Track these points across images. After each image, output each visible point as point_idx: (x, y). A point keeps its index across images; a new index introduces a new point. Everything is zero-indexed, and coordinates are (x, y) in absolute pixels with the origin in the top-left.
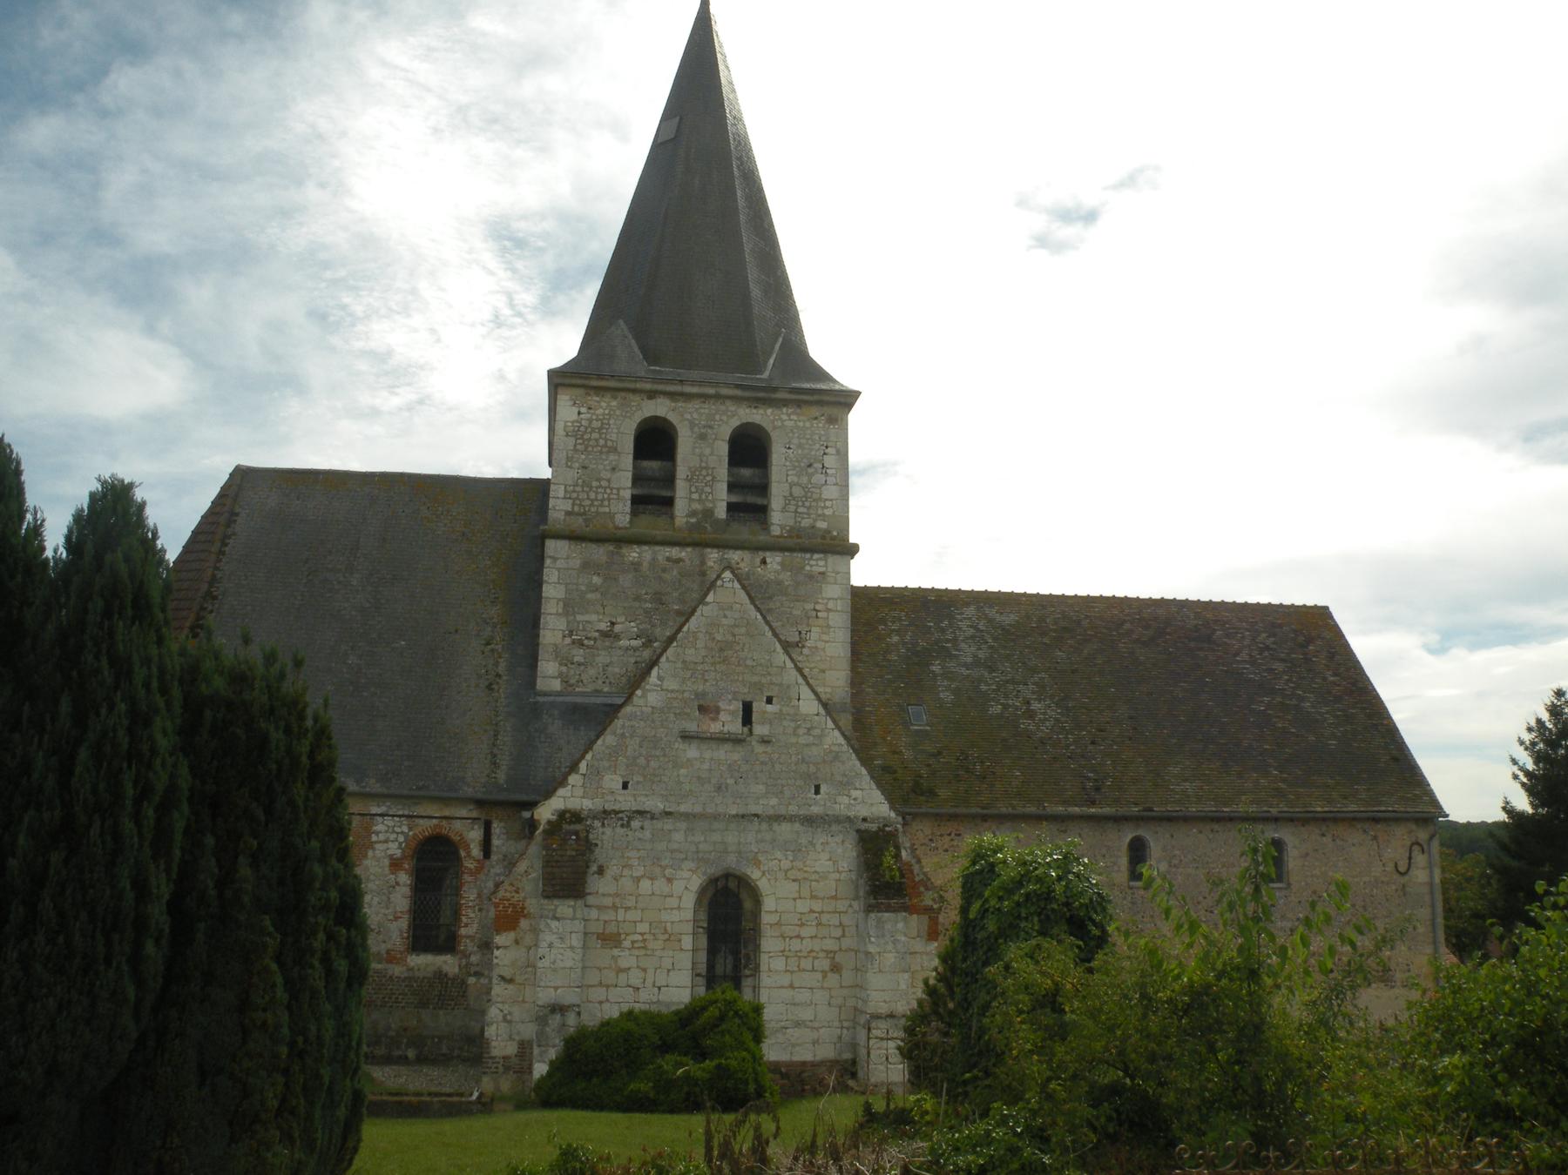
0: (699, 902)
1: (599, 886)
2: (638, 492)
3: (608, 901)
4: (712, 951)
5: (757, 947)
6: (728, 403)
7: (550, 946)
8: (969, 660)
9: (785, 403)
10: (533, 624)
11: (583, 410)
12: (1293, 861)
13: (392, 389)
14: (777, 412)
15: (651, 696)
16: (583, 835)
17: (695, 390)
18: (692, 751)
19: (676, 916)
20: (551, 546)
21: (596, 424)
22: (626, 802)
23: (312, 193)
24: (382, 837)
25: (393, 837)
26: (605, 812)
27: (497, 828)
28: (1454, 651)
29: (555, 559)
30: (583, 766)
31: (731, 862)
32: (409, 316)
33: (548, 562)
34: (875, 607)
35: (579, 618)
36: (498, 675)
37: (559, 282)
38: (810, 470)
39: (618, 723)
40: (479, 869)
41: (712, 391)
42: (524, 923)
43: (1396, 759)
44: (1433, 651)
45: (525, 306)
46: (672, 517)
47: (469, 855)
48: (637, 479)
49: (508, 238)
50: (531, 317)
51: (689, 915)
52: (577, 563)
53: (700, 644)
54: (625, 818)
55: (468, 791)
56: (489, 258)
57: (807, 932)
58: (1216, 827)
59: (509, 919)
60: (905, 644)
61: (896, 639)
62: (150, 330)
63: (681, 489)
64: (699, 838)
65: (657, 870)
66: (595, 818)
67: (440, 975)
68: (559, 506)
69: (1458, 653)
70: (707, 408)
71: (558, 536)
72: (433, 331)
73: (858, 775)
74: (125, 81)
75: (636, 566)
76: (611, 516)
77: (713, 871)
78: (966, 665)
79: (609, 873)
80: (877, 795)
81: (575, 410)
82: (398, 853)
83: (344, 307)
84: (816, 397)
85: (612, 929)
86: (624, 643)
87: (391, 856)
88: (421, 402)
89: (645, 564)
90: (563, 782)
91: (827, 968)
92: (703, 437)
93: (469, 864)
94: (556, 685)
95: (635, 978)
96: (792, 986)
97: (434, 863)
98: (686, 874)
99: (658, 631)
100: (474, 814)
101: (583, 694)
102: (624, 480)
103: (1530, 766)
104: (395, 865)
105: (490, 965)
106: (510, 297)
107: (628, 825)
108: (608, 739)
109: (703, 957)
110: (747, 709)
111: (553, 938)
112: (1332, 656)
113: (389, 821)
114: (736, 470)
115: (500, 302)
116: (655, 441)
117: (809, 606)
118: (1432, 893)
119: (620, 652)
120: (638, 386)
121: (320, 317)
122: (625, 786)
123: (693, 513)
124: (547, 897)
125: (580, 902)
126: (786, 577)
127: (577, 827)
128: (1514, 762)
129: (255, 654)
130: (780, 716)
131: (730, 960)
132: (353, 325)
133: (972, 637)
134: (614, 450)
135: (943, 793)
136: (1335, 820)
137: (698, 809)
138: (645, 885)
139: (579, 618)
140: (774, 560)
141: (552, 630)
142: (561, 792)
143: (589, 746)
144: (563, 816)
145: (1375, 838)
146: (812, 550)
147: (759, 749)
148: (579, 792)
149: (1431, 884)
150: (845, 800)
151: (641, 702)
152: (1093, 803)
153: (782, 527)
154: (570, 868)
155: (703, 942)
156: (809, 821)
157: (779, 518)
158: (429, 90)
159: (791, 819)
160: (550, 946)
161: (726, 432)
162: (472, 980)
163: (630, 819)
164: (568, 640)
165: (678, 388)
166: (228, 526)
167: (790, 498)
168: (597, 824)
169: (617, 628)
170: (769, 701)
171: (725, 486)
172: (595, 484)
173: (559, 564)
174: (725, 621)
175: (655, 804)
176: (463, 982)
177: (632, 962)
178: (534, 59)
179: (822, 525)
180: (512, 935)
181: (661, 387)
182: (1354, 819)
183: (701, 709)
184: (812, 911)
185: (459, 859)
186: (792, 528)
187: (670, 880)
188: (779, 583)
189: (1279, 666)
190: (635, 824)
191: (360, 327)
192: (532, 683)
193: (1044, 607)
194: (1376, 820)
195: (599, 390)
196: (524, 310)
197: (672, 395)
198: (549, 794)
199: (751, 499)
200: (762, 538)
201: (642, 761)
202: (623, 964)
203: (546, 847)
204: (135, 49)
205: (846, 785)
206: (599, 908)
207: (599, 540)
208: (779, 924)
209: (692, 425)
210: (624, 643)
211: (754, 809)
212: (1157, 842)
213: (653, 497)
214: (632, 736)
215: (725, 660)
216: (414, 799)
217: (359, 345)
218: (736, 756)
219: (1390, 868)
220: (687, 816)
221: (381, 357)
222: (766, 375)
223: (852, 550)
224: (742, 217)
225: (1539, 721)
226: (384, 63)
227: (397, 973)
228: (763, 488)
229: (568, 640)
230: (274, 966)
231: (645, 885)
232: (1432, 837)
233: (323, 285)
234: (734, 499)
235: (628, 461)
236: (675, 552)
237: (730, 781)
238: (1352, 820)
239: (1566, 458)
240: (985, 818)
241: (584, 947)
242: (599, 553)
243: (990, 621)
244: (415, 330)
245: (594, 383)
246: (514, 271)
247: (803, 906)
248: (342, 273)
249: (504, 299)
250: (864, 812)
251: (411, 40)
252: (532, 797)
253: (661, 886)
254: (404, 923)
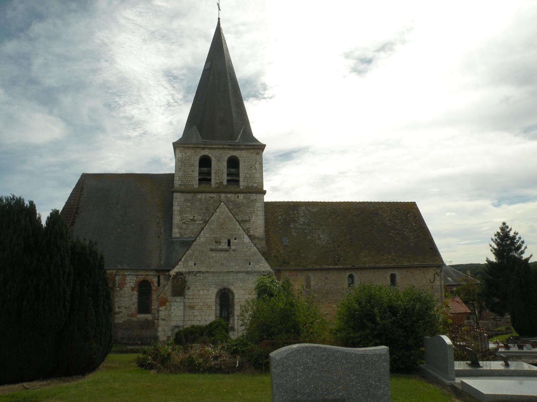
0: (217, 296)
1: (188, 293)
2: (200, 177)
3: (191, 297)
4: (221, 310)
5: (234, 308)
7: (174, 310)
8: (302, 223)
9: (243, 149)
10: (171, 217)
12: (398, 279)
13: (134, 129)
15: (201, 239)
16: (183, 279)
17: (216, 147)
18: (214, 254)
19: (210, 300)
20: (175, 195)
21: (187, 158)
22: (195, 269)
23: (103, 64)
24: (129, 281)
27: (162, 278)
28: (503, 205)
29: (176, 199)
30: (183, 259)
31: (225, 285)
32: (139, 104)
33: (174, 199)
34: (273, 208)
36: (161, 233)
37: (188, 91)
39: (193, 247)
40: (157, 289)
41: (221, 147)
42: (168, 304)
43: (431, 248)
44: (495, 206)
45: (178, 99)
46: (211, 184)
48: (200, 174)
49: (171, 76)
50: (180, 103)
51: (214, 300)
52: (183, 199)
54: (195, 273)
55: (153, 267)
56: (164, 83)
58: (375, 271)
59: (163, 302)
60: (282, 219)
61: (280, 217)
62: (51, 113)
63: (213, 176)
64: (216, 278)
65: (204, 288)
67: (147, 320)
68: (177, 183)
69: (505, 206)
70: (220, 152)
71: (177, 192)
72: (147, 109)
73: (261, 259)
74: (38, 28)
75: (200, 200)
76: (193, 185)
77: (220, 288)
78: (301, 225)
79: (191, 289)
80: (267, 265)
82: (133, 286)
83: (116, 102)
84: (253, 147)
85: (192, 304)
86: (198, 222)
87: (132, 287)
88: (144, 133)
90: (177, 264)
92: (219, 160)
93: (154, 288)
95: (199, 318)
97: (144, 289)
98: (213, 289)
100: (155, 274)
101: (186, 238)
102: (196, 174)
103: (496, 247)
104: (133, 289)
105: (158, 316)
106: (173, 96)
107: (196, 275)
108: (190, 251)
109: (218, 312)
110: (229, 241)
111: (175, 307)
112: (415, 217)
113: (130, 277)
114: (229, 170)
115: (170, 98)
116: (205, 162)
117: (252, 209)
118: (441, 288)
120: (199, 146)
121: (108, 106)
122: (195, 264)
123: (217, 183)
124: (173, 296)
125: (183, 297)
126: (245, 201)
127: (181, 276)
128: (491, 246)
129: (87, 243)
131: (226, 312)
132: (120, 108)
133: (304, 216)
134: (193, 165)
135: (292, 263)
136: (411, 267)
137: (216, 270)
138: (201, 292)
139: (184, 215)
140: (241, 196)
141: (177, 219)
142: (177, 267)
143: (185, 254)
144: (179, 274)
145: (424, 272)
146: (252, 193)
147: (233, 253)
148: (182, 266)
149: (441, 285)
150: (258, 266)
151: (199, 241)
152: (337, 265)
153: (243, 186)
154: (180, 288)
155: (218, 307)
156: (247, 272)
157: (242, 184)
158: (141, 27)
159: (242, 272)
160: (174, 310)
161: (226, 159)
162: (156, 321)
163: (196, 274)
164: (181, 222)
165: (211, 146)
166: (81, 191)
167: (245, 177)
168: (187, 275)
169: (195, 218)
170: (235, 239)
171: (226, 175)
173: (178, 200)
175: (204, 269)
176: (153, 322)
177: (198, 314)
178: (176, 15)
179: (255, 185)
180: (164, 307)
181: (206, 146)
182: (417, 267)
183: (216, 242)
185: (151, 287)
186: (246, 187)
187: (208, 291)
188: (243, 203)
189: (398, 221)
190: (198, 275)
191: (122, 109)
192: (171, 235)
193: (326, 206)
194: (424, 267)
195: (188, 148)
196: (178, 101)
197: (210, 148)
198: (174, 267)
199: (234, 178)
200: (237, 190)
201: (199, 257)
202: (196, 314)
203: (173, 282)
204: (41, 17)
205: (258, 262)
206: (189, 299)
207: (189, 192)
208: (239, 302)
209: (216, 157)
210: (198, 222)
211: (231, 270)
212: (357, 276)
213: (205, 178)
216: (138, 270)
217: (122, 115)
218: (226, 255)
219: (428, 281)
220: (213, 272)
221: (130, 119)
222: (237, 141)
223: (264, 192)
224: (230, 92)
225: (498, 233)
226: (125, 18)
228: (238, 175)
229: (181, 222)
230: (92, 307)
231: (201, 292)
232: (441, 271)
233: (109, 95)
234: (229, 178)
235: (197, 168)
236: (212, 195)
237: (225, 262)
238: (416, 267)
239: (536, 138)
240: (304, 270)
241: (184, 309)
242: (189, 196)
243: (309, 211)
244: (141, 109)
245: (187, 146)
246: (174, 87)
248: (115, 90)
249: (171, 97)
250: (263, 270)
251: (134, 9)
252: (169, 268)
253: (205, 292)
254: (136, 306)
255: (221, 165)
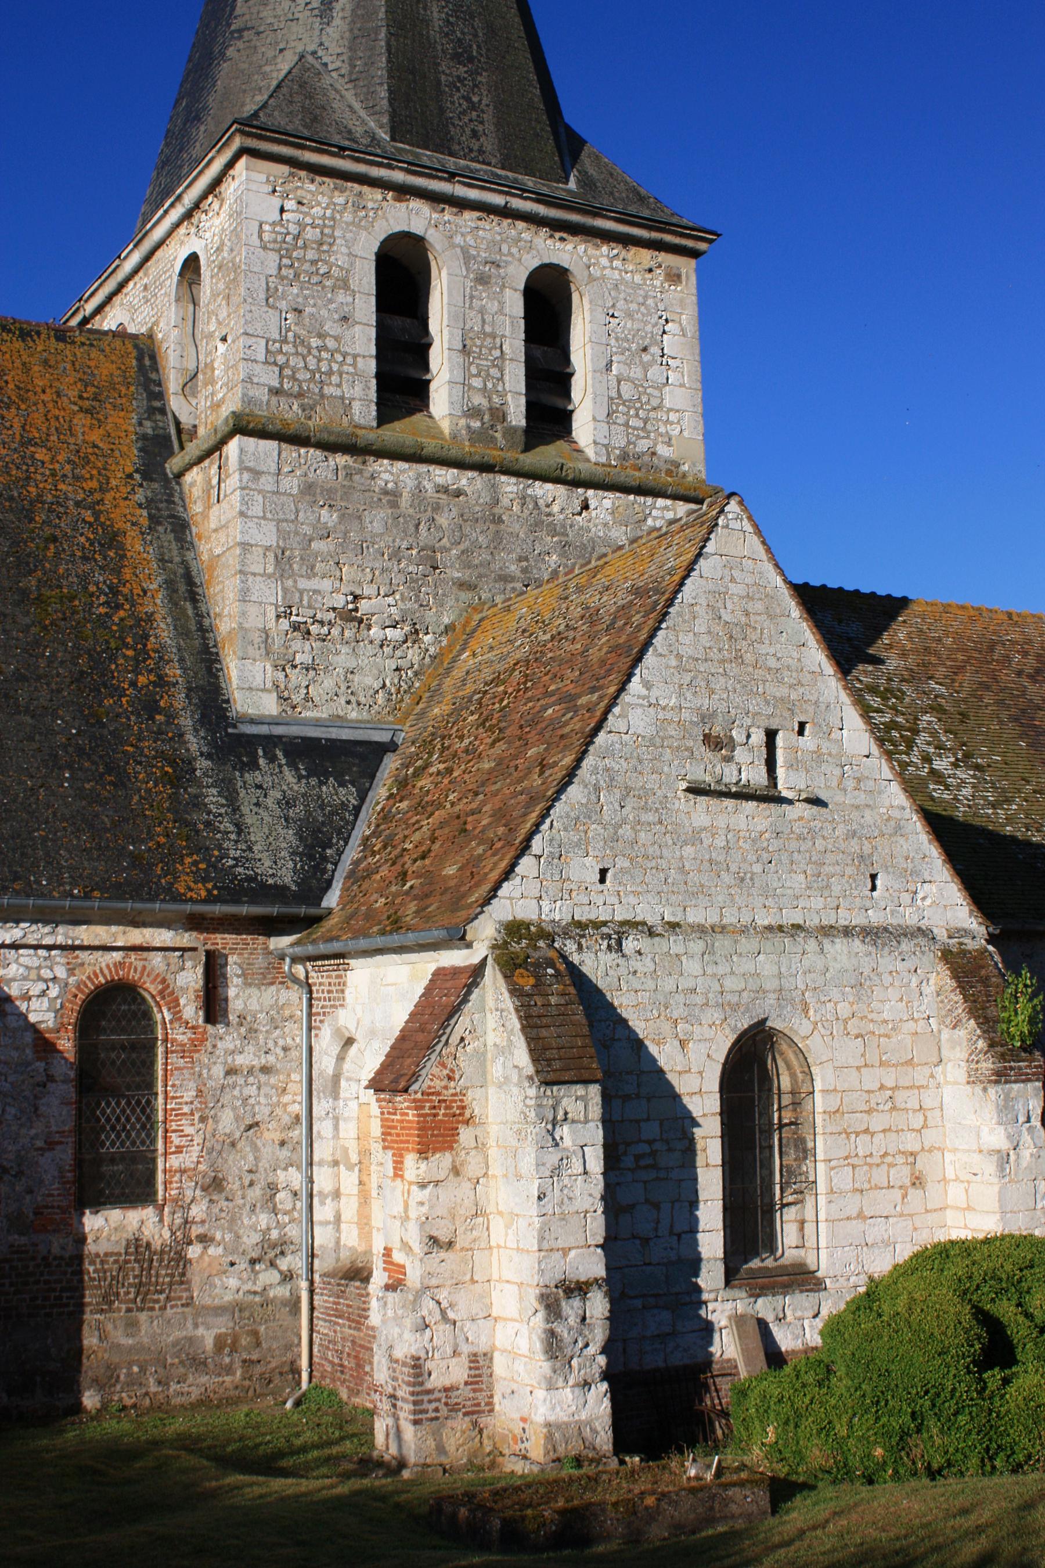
6: (521, 225)
11: (290, 205)
14: (591, 251)
17: (473, 194)
18: (702, 813)
21: (310, 234)
25: (38, 987)
26: (579, 925)
35: (303, 584)
38: (646, 357)
40: (198, 1043)
41: (498, 200)
42: (465, 1135)
47: (177, 1017)
52: (291, 484)
53: (700, 627)
57: (877, 1122)
66: (566, 934)
70: (493, 228)
75: (392, 496)
81: (276, 202)
89: (406, 495)
91: (907, 1182)
92: (482, 280)
94: (269, 706)
96: (861, 1216)
99: (430, 616)
101: (317, 723)
113: (26, 957)
116: (402, 278)
119: (370, 650)
123: (474, 412)
130: (818, 756)
137: (713, 919)
139: (303, 584)
156: (872, 934)
159: (847, 932)
162: (193, 1252)
164: (284, 624)
169: (364, 606)
172: (315, 342)
174: (734, 589)
175: (648, 911)
176: (181, 1260)
184: (882, 1087)
214: (610, 787)
215: (739, 659)
220: (701, 930)
227: (56, 1250)
237: (757, 868)
247: (870, 1079)
255: (493, 307)
